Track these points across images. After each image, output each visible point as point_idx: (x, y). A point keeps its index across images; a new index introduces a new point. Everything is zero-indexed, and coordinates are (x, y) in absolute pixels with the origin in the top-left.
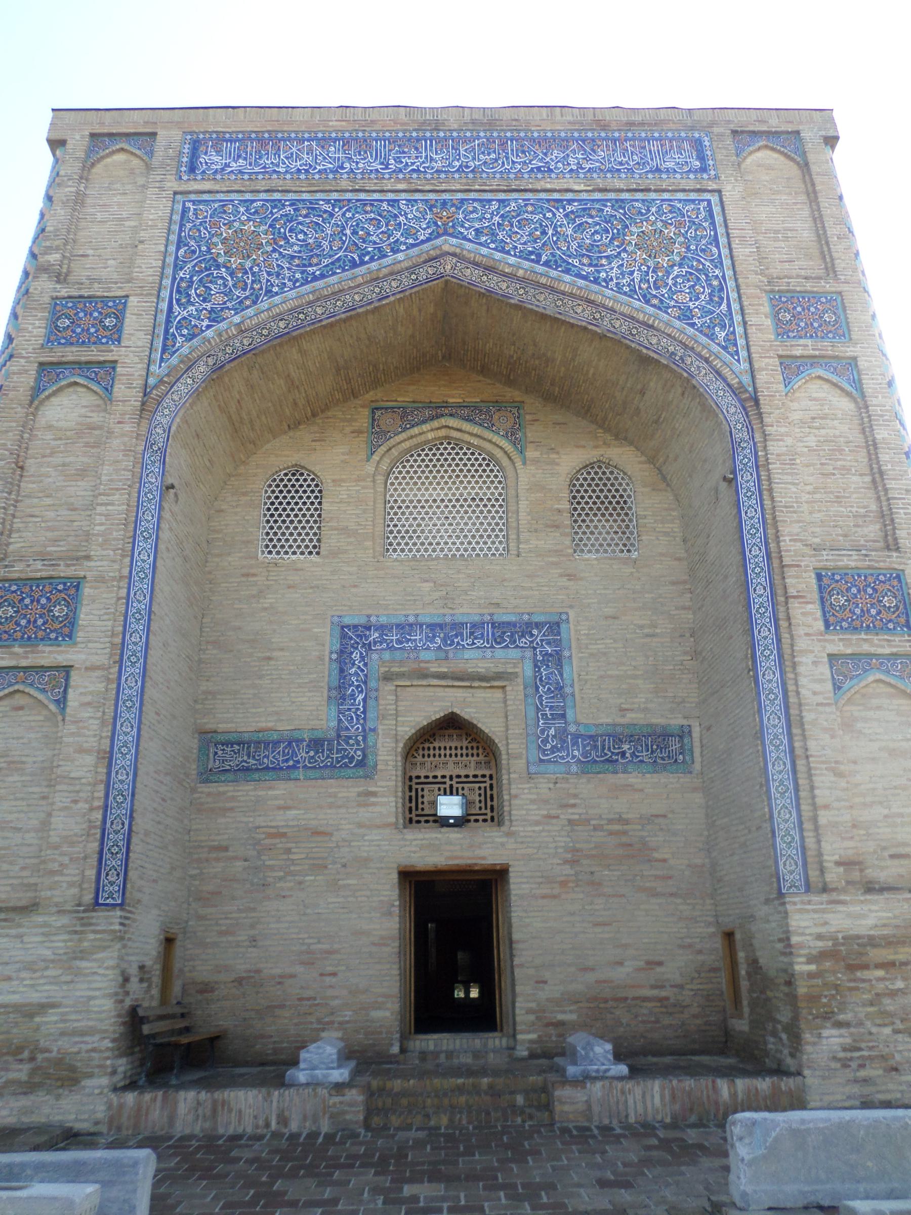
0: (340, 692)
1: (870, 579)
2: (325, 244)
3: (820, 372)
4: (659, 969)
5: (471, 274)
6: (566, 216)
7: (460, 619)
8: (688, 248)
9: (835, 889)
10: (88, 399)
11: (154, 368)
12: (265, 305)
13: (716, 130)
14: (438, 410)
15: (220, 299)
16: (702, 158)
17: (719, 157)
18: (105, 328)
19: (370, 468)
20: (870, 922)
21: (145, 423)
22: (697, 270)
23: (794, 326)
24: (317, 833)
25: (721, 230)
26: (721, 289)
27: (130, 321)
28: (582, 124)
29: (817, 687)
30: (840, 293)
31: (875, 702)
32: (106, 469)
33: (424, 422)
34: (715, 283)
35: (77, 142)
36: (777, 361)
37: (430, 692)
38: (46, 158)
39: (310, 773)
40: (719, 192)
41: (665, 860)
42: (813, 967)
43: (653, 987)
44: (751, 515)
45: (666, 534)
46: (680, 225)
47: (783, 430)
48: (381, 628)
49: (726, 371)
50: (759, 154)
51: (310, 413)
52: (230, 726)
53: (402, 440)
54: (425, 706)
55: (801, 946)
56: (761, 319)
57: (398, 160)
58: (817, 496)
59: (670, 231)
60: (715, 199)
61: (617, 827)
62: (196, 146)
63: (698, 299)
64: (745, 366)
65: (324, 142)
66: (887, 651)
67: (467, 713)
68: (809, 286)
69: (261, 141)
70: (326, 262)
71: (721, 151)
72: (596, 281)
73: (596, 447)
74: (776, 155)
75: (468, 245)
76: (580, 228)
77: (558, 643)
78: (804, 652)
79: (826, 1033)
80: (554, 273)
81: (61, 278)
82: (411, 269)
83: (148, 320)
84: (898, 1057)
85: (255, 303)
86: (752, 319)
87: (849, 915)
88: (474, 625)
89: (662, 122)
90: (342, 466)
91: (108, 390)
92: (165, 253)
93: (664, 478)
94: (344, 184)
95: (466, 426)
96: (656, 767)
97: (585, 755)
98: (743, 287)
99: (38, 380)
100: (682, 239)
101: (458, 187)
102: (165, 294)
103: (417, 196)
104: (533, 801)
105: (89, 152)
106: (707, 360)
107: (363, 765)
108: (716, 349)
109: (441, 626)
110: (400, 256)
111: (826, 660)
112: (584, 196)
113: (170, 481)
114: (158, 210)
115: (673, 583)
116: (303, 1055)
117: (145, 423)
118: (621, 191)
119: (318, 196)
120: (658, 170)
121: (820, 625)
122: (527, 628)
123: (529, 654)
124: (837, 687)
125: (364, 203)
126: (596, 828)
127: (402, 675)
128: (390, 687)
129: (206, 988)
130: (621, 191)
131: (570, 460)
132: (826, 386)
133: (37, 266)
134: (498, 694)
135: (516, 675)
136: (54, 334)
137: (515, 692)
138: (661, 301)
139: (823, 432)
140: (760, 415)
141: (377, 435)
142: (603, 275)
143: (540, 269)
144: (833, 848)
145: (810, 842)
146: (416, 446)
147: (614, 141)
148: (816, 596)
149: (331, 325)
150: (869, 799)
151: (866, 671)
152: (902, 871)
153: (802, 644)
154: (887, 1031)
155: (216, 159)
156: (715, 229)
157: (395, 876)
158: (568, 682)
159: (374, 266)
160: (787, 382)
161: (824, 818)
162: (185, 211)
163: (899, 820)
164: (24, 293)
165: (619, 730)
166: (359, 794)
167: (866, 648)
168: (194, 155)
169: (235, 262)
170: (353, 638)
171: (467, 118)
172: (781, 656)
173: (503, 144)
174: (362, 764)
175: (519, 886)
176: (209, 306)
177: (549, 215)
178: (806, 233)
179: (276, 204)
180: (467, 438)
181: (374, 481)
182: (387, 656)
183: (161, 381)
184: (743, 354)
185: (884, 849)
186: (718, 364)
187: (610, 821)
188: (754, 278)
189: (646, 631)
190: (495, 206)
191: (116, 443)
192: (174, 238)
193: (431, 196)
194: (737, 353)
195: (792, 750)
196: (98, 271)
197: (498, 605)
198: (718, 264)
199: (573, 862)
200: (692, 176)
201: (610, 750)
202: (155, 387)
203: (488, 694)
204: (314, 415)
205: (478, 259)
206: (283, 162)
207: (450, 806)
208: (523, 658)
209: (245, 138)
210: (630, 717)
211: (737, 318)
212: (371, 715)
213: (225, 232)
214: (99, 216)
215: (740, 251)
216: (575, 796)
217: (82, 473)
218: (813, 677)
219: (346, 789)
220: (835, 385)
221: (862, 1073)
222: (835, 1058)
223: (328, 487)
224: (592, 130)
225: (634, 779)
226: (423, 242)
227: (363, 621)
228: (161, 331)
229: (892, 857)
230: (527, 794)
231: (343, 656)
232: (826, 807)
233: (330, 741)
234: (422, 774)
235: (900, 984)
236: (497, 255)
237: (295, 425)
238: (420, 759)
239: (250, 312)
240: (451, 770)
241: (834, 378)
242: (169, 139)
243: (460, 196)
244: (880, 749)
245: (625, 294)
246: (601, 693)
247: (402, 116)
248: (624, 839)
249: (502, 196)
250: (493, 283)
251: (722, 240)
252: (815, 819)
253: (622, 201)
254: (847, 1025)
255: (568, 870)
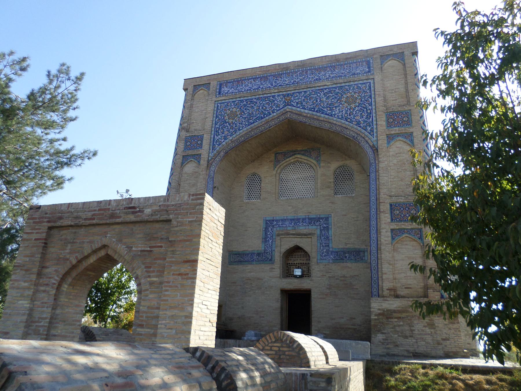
0: (265, 240)
1: (408, 205)
2: (254, 113)
3: (400, 138)
4: (354, 320)
5: (295, 117)
6: (324, 94)
7: (299, 217)
8: (361, 101)
9: (386, 297)
10: (195, 165)
11: (210, 155)
12: (238, 133)
13: (375, 56)
14: (294, 152)
15: (226, 133)
16: (369, 68)
17: (375, 66)
18: (198, 144)
19: (274, 172)
20: (395, 306)
21: (208, 171)
22: (364, 108)
23: (393, 123)
24: (259, 279)
25: (373, 92)
26: (370, 113)
27: (204, 142)
28: (331, 61)
29: (386, 239)
30: (410, 110)
31: (405, 243)
32: (199, 184)
33: (290, 157)
34: (369, 111)
35: (191, 89)
36: (385, 136)
37: (290, 239)
38: (184, 93)
39: (257, 262)
40: (374, 79)
41: (357, 289)
42: (376, 317)
43: (353, 325)
44: (373, 187)
45: (363, 188)
46: (360, 92)
47: (384, 159)
48: (277, 221)
49: (369, 141)
50: (390, 62)
51: (257, 157)
52: (236, 250)
53: (284, 163)
54: (288, 243)
55: (373, 311)
56: (382, 122)
57: (275, 82)
58: (395, 179)
59: (356, 95)
60: (372, 81)
61: (342, 279)
62: (221, 85)
63: (363, 117)
64: (375, 139)
65: (255, 79)
66: (410, 227)
67: (301, 245)
68: (400, 109)
69: (238, 81)
70: (254, 118)
71: (376, 64)
72: (331, 116)
73: (342, 161)
74: (396, 62)
75: (294, 108)
76: (328, 98)
77: (328, 224)
78: (383, 228)
79: (378, 335)
80: (319, 114)
81: (187, 131)
82: (278, 118)
83: (208, 141)
84: (398, 343)
85: (235, 133)
86: (379, 123)
87: (389, 304)
88: (303, 219)
89: (357, 56)
90: (267, 172)
91: (199, 162)
92: (213, 121)
93: (364, 170)
94: (260, 93)
95: (303, 157)
96: (356, 261)
97: (334, 257)
98: (377, 112)
99: (183, 160)
100: (360, 97)
101: (292, 89)
102: (213, 133)
103: (281, 93)
104: (318, 271)
105: (194, 91)
106: (364, 138)
107: (271, 261)
108: (367, 134)
109: (294, 219)
110: (275, 114)
111: (390, 231)
112: (330, 86)
113: (215, 185)
114: (211, 107)
115: (364, 204)
116: (246, 333)
117: (208, 171)
118: (342, 83)
119: (253, 97)
120: (354, 74)
121: (389, 220)
122: (318, 219)
123: (319, 227)
124: (393, 239)
125: (265, 98)
126: (337, 279)
127: (282, 234)
128: (279, 238)
129: (231, 319)
130: (342, 83)
131: (334, 165)
132: (402, 143)
133: (182, 128)
134: (310, 239)
135: (315, 233)
136: (186, 148)
137: (315, 239)
138: (351, 120)
139: (399, 158)
140: (378, 154)
141: (277, 161)
142: (334, 113)
143: (315, 113)
144: (386, 285)
145: (380, 283)
146: (289, 164)
147: (341, 65)
148: (389, 212)
149: (257, 136)
150: (400, 271)
151: (403, 234)
152: (408, 292)
153: (383, 226)
154: (396, 336)
155: (226, 89)
156: (371, 93)
157: (279, 291)
158: (330, 235)
159: (267, 118)
160: (389, 143)
161: (384, 277)
162: (218, 106)
163: (409, 278)
164: (179, 136)
165: (345, 250)
166: (270, 269)
167: (403, 227)
168: (220, 89)
169: (230, 121)
170: (269, 223)
171: (296, 65)
172: (377, 229)
173: (307, 72)
174: (271, 260)
175: (314, 295)
176: (224, 135)
177: (319, 95)
178: (403, 90)
179: (242, 101)
180: (303, 160)
181: (276, 176)
182: (278, 229)
183: (212, 158)
184: (375, 135)
185: (403, 286)
186: (367, 139)
187: (341, 277)
188: (382, 108)
189: (355, 219)
190: (303, 93)
191: (201, 177)
192: (215, 115)
193: (285, 93)
194: (373, 134)
195: (378, 257)
196: (196, 127)
197: (310, 213)
198: (371, 104)
199: (329, 289)
200: (365, 74)
201: (342, 256)
202: (211, 160)
203: (307, 239)
204: (258, 157)
205: (297, 112)
206: (242, 88)
207: (298, 272)
208: (317, 229)
209: (233, 82)
210: (348, 246)
211: (374, 123)
212: (273, 246)
213: (228, 112)
214: (196, 111)
215: (378, 99)
216: (331, 269)
217: (194, 185)
218: (385, 236)
219: (266, 267)
220: (405, 142)
221: (387, 346)
222: (380, 342)
223: (263, 179)
224: (334, 63)
225: (349, 264)
226: (281, 108)
227: (272, 219)
228: (212, 144)
229: (405, 288)
230: (316, 270)
231: (266, 229)
232: (386, 274)
233: (262, 254)
234: (291, 262)
235: (401, 323)
236: (303, 111)
237: (253, 161)
238: (290, 258)
239: (234, 136)
240: (299, 261)
241: (405, 140)
242: (214, 84)
243: (293, 92)
244: (405, 257)
245: (340, 119)
246: (339, 240)
247: (277, 68)
248: (345, 282)
249: (305, 90)
250: (301, 119)
251: (373, 96)
252: (382, 277)
253: (342, 86)
254: (385, 333)
255: (328, 291)
